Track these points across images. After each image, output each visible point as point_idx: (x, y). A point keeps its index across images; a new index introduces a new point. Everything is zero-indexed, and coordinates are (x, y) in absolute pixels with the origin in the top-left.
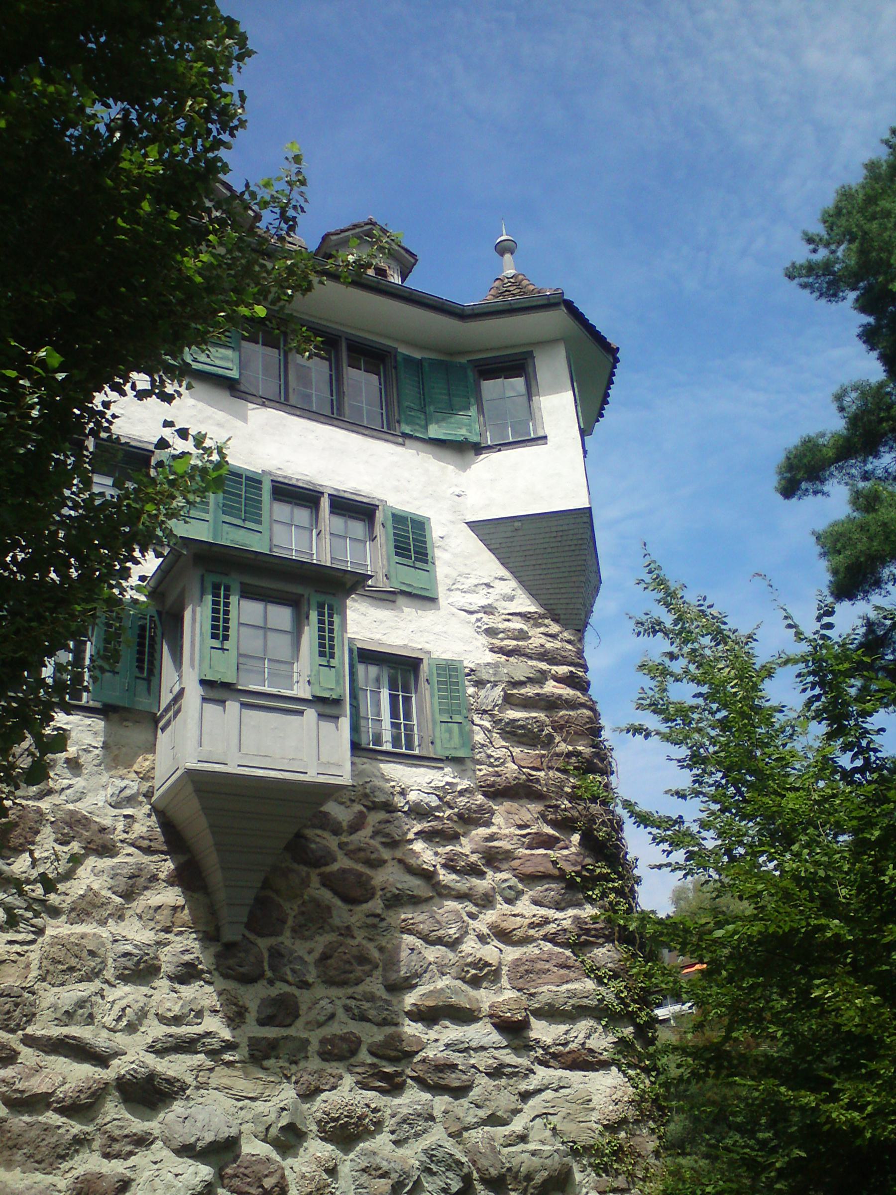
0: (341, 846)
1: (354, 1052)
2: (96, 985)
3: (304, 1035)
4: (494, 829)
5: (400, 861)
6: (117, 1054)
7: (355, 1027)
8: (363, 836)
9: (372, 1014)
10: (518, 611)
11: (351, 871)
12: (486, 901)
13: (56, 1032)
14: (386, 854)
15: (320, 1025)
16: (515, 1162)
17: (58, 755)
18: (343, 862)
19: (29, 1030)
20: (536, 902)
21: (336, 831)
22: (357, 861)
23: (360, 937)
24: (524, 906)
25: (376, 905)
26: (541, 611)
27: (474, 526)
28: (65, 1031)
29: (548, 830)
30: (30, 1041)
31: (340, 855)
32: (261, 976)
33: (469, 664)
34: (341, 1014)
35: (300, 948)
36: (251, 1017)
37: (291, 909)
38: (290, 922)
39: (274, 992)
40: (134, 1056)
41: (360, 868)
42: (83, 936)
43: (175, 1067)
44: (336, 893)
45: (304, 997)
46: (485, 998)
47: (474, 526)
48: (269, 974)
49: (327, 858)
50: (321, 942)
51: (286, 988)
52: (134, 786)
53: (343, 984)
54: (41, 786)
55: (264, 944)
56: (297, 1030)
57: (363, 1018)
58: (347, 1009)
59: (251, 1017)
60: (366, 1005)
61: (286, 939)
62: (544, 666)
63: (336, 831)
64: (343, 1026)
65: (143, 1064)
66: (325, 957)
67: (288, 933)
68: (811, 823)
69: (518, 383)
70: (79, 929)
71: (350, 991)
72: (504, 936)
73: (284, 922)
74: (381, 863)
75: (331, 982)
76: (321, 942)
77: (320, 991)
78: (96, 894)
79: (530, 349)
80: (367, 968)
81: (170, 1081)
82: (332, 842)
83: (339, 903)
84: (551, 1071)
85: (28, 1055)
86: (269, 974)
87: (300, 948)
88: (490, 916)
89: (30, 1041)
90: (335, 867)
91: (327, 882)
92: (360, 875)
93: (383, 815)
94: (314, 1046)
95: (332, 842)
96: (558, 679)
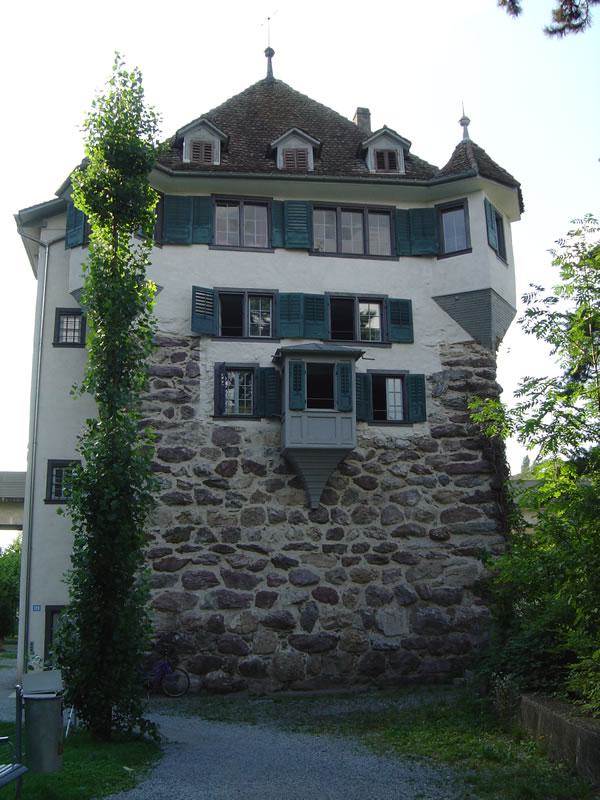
0: (363, 466)
1: (367, 550)
2: (263, 526)
3: (345, 543)
4: (438, 453)
5: (391, 471)
6: (273, 551)
7: (368, 540)
8: (374, 460)
9: (375, 535)
10: (34, 546)
11: (367, 477)
12: (432, 485)
13: (248, 543)
14: (384, 468)
15: (352, 540)
16: (437, 592)
17: (177, 572)
18: (364, 473)
19: (239, 543)
20: (457, 485)
21: (361, 459)
22: (371, 472)
23: (371, 504)
24: (451, 487)
25: (378, 490)
26: (471, 339)
27: (436, 299)
28: (252, 543)
29: (466, 451)
30: (238, 546)
31: (362, 470)
32: (328, 520)
33: (428, 374)
34: (362, 535)
35: (345, 509)
36: (324, 537)
37: (340, 493)
38: (341, 499)
39: (333, 527)
40: (277, 551)
41: (372, 475)
42: (256, 508)
43: (293, 555)
44: (360, 486)
45: (346, 529)
46: (429, 527)
47: (436, 299)
48: (331, 520)
49: (356, 472)
50: (353, 507)
51: (339, 526)
52: (518, 433)
53: (363, 523)
54: (183, 544)
55: (329, 508)
56: (343, 542)
57: (372, 536)
58: (365, 533)
59: (324, 537)
60: (372, 532)
61: (339, 506)
62: (471, 369)
63: (361, 459)
64: (362, 539)
65: (281, 555)
66: (355, 513)
67: (340, 504)
68: (385, 447)
69: (462, 212)
70: (255, 505)
71: (366, 526)
72: (438, 499)
73: (337, 499)
74: (382, 472)
75: (357, 523)
76: (353, 507)
77: (353, 526)
78: (260, 493)
79: (464, 197)
80: (374, 517)
81: (292, 560)
82: (359, 465)
83: (361, 490)
84: (458, 557)
85: (239, 551)
86: (331, 520)
87: (345, 509)
88: (434, 491)
89: (238, 546)
90: (360, 476)
91: (356, 481)
92: (371, 478)
93: (383, 451)
94: (350, 548)
95: (359, 465)
96: (478, 374)
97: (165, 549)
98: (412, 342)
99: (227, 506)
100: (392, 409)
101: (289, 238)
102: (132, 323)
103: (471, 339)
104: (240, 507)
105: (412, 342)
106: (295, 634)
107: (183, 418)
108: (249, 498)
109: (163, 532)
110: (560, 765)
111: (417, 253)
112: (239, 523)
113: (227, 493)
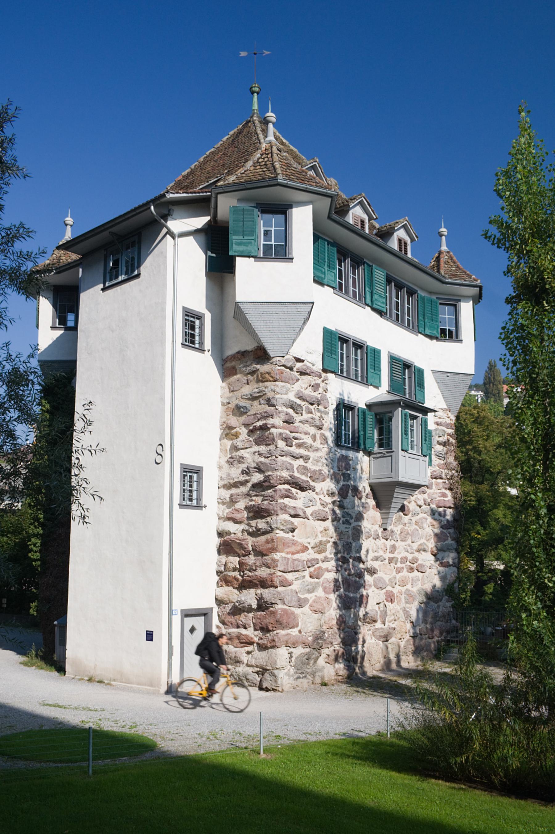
9: (409, 550)
26: (446, 407)
45: (397, 544)
97: (314, 559)
98: (147, 640)
99: (343, 523)
100: (115, 728)
101: (376, 300)
102: (40, 528)
103: (446, 407)
104: (350, 524)
105: (147, 640)
106: (376, 627)
107: (321, 443)
108: (354, 517)
109: (312, 545)
110: (487, 690)
111: (428, 332)
112: (351, 538)
113: (343, 512)
